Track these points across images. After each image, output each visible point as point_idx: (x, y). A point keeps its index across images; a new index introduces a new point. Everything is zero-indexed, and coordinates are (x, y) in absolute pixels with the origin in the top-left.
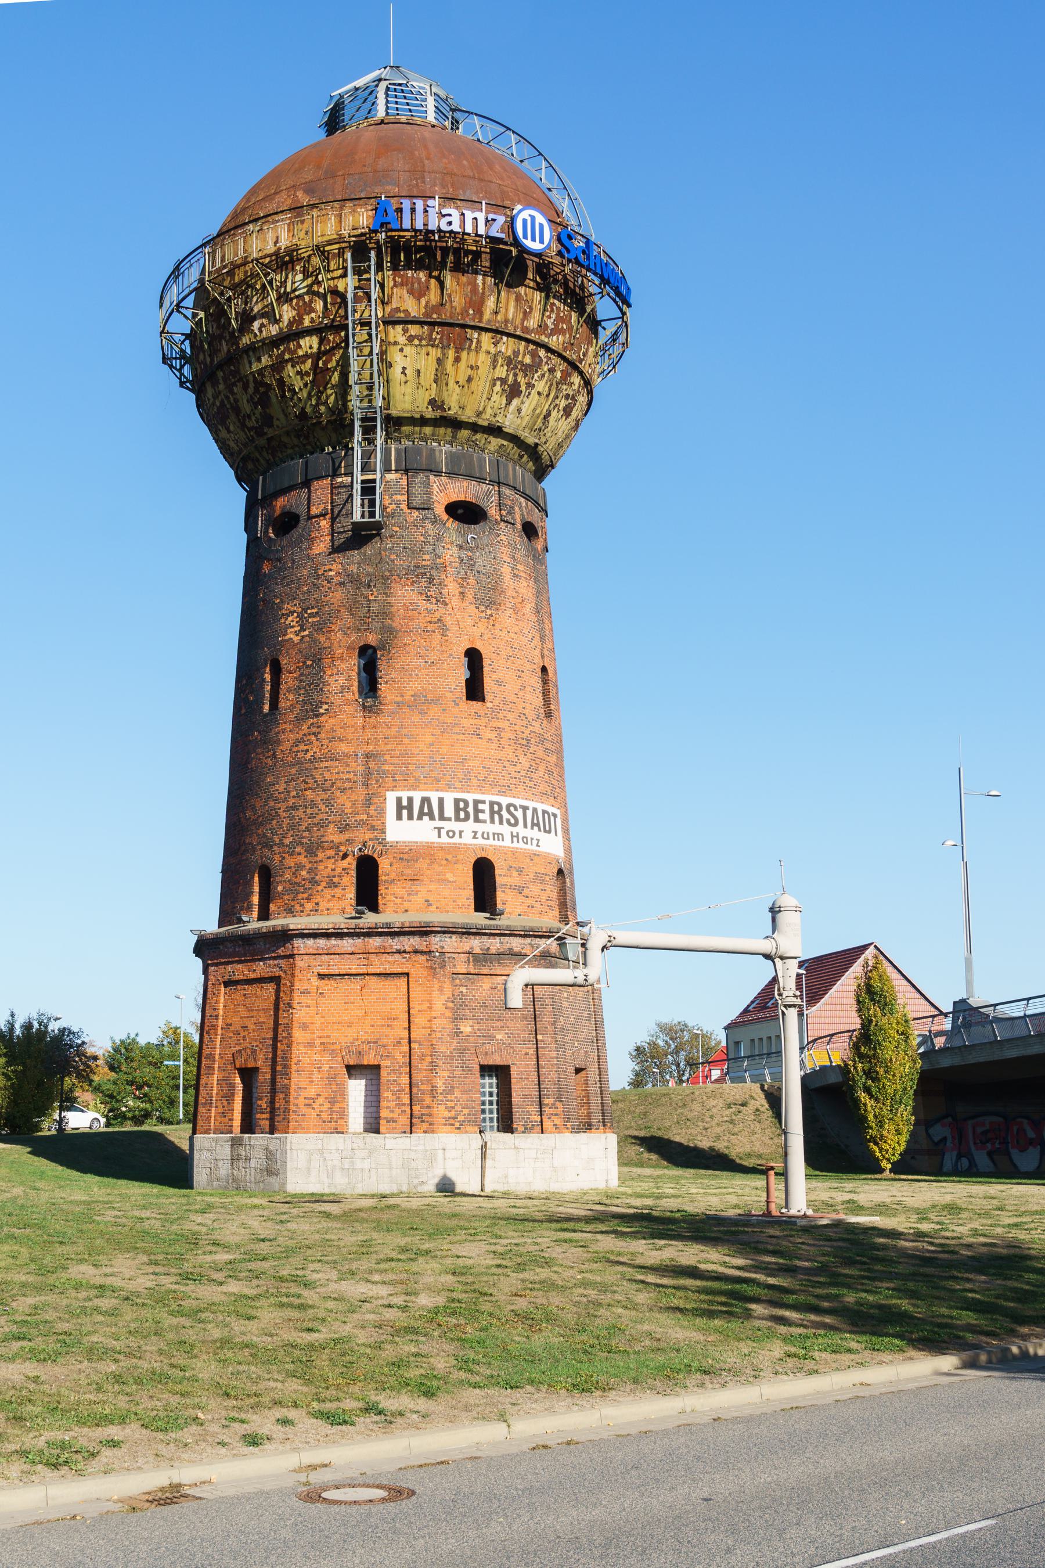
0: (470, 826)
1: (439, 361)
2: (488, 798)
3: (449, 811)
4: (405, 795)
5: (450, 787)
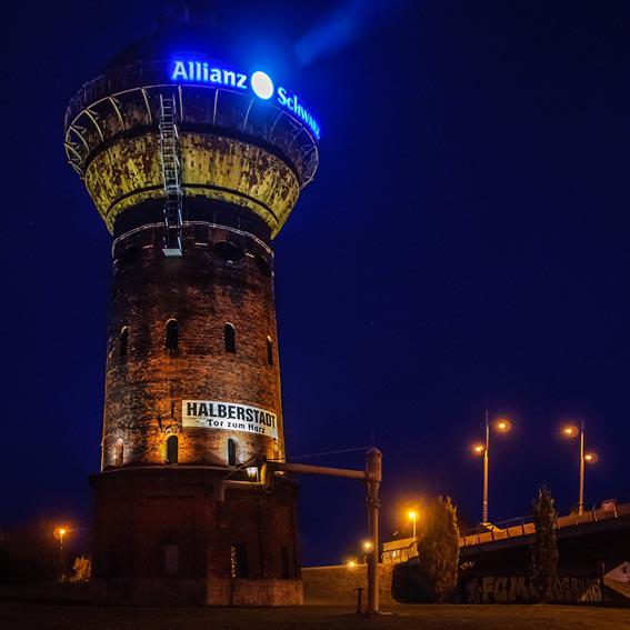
0: (226, 421)
1: (211, 160)
2: (237, 405)
3: (235, 415)
4: (192, 402)
5: (216, 398)
